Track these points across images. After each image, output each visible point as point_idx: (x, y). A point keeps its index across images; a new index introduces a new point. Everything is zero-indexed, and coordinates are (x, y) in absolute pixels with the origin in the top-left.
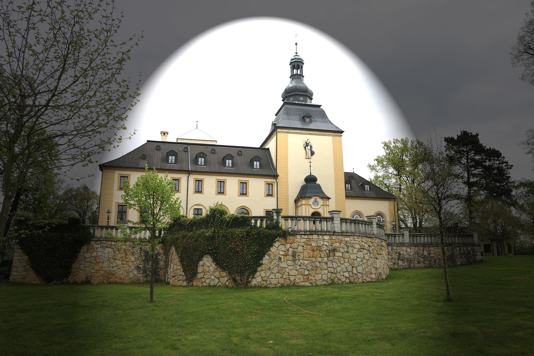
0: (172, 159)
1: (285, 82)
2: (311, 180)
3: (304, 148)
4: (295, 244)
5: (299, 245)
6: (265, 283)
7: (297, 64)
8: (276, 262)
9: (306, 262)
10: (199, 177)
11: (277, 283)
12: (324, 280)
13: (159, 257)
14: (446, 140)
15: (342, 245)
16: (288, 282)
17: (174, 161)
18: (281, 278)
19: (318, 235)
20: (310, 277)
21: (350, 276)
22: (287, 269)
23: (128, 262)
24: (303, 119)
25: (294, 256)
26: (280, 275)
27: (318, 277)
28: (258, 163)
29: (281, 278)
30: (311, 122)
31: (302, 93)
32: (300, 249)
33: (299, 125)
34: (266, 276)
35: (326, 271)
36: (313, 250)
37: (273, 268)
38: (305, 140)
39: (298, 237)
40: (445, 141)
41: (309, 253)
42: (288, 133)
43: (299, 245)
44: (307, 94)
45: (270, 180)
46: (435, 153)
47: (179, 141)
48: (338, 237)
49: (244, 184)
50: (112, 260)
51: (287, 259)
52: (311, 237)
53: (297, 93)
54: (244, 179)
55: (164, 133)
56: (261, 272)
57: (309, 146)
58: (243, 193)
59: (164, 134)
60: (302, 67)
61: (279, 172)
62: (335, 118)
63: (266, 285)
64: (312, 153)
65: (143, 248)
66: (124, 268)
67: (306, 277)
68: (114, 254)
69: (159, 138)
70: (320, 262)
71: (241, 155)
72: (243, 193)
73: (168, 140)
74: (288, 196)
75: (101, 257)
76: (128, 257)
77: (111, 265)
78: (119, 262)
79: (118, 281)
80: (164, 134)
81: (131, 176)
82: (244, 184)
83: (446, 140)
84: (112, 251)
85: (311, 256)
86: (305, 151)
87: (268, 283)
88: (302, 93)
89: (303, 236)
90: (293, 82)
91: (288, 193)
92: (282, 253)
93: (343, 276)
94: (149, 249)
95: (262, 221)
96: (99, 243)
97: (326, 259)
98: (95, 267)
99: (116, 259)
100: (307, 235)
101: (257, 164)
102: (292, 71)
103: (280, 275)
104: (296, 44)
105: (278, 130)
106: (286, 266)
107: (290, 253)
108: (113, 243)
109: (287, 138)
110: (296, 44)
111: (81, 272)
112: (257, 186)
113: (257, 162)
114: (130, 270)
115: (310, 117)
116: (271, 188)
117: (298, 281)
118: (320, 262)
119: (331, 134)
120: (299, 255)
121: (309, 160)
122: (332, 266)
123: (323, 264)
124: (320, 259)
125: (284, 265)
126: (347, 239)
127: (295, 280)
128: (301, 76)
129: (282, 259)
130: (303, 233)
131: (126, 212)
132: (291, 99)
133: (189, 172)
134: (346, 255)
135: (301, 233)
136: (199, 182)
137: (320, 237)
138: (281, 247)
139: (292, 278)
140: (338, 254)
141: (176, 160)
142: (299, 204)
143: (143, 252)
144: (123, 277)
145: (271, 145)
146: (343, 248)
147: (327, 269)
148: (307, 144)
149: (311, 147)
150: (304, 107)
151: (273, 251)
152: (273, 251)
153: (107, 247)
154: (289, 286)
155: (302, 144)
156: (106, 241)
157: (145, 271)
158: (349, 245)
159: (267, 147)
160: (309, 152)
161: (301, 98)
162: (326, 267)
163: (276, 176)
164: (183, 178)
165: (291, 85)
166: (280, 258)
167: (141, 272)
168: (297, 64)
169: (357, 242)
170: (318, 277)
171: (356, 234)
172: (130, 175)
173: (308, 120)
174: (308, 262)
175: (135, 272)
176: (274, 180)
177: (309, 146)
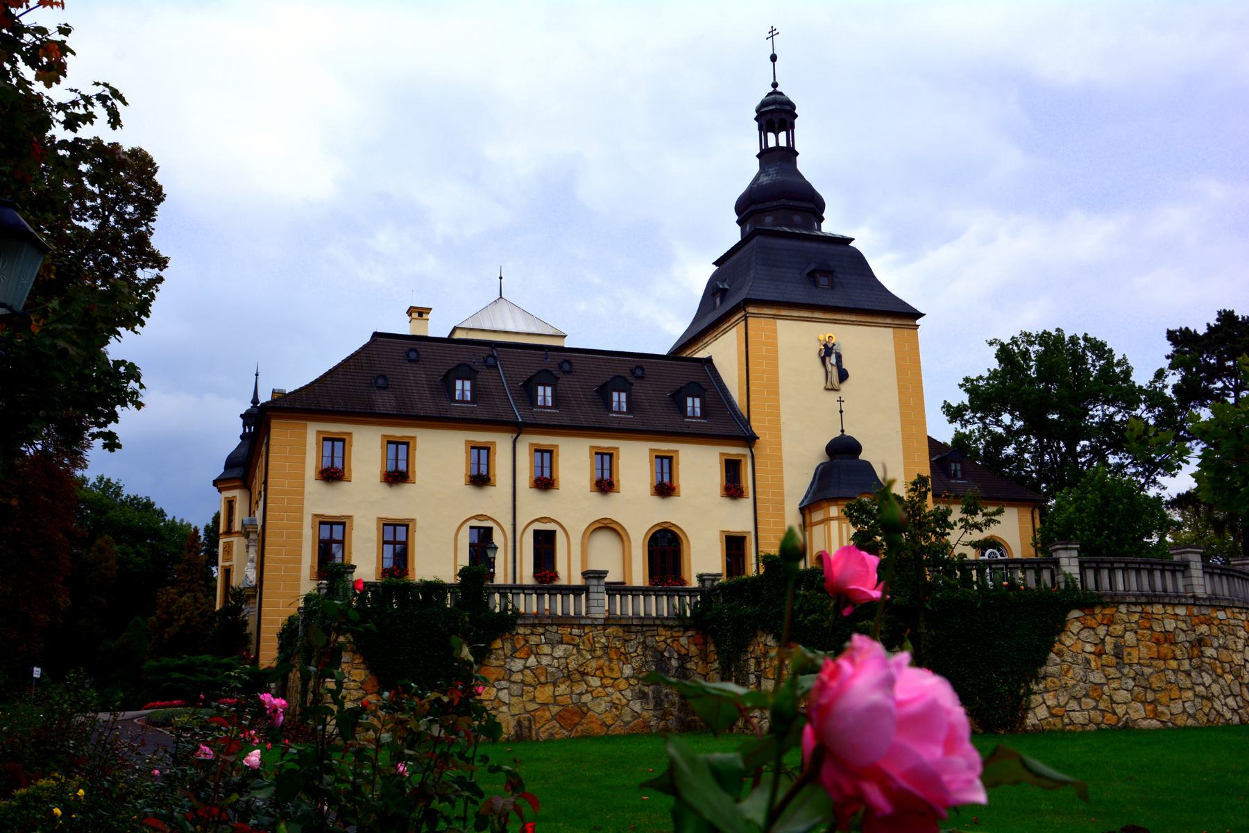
0: (463, 388)
1: (744, 170)
2: (843, 451)
3: (818, 362)
4: (1118, 627)
5: (1126, 630)
6: (1058, 721)
7: (776, 114)
8: (1078, 670)
9: (1147, 671)
10: (545, 441)
11: (1086, 721)
12: (1189, 715)
13: (689, 666)
14: (1171, 335)
15: (1215, 630)
16: (1111, 719)
17: (549, 399)
18: (1095, 708)
19: (1164, 605)
20: (1160, 708)
21: (1240, 708)
22: (1106, 688)
23: (615, 679)
24: (812, 277)
25: (1119, 656)
26: (1092, 703)
27: (1177, 708)
28: (468, 384)
29: (1095, 708)
30: (832, 286)
31: (798, 204)
32: (1130, 637)
33: (799, 296)
34: (1059, 705)
35: (1190, 694)
36: (1158, 642)
37: (1074, 686)
38: (823, 337)
39: (1123, 609)
40: (1169, 339)
41: (1149, 648)
42: (776, 317)
43: (1126, 630)
44: (811, 204)
45: (733, 451)
46: (1142, 378)
47: (459, 335)
48: (1204, 611)
49: (666, 462)
50: (578, 676)
51: (1104, 662)
52: (1149, 609)
53: (783, 201)
54: (664, 447)
55: (419, 313)
56: (1046, 696)
57: (833, 356)
58: (665, 489)
59: (420, 314)
60: (793, 127)
61: (756, 426)
62: (891, 273)
63: (1060, 726)
64: (843, 376)
65: (649, 641)
66: (607, 695)
67: (1150, 708)
68: (581, 661)
69: (402, 326)
70: (1174, 671)
71: (415, 361)
72: (665, 489)
73: (432, 333)
74: (782, 494)
75: (549, 669)
76: (616, 667)
77: (577, 689)
78: (595, 682)
79: (597, 729)
80: (420, 314)
81: (354, 437)
82: (666, 462)
83: (1171, 335)
84: (575, 651)
85: (1155, 655)
86: (822, 371)
87: (1066, 721)
88: (798, 204)
89: (1133, 608)
90: (771, 170)
91: (782, 487)
92: (1089, 648)
93: (1226, 705)
94: (663, 645)
95: (981, 572)
96: (541, 630)
97: (1186, 665)
98: (537, 694)
99: (588, 674)
100: (1140, 604)
101: (693, 405)
102: (763, 140)
103: (1092, 703)
104: (774, 58)
105: (751, 310)
106: (1104, 681)
107: (1109, 647)
108: (575, 631)
109: (775, 331)
110: (774, 58)
111: (504, 709)
112: (700, 465)
113: (669, 397)
114: (624, 701)
115: (828, 272)
116: (483, 460)
117: (1134, 716)
118: (1174, 671)
119: (889, 321)
120: (1129, 654)
121: (835, 396)
122: (1199, 681)
123: (1182, 676)
124: (1174, 664)
125: (1097, 677)
126: (1221, 615)
127: (1127, 713)
128: (789, 153)
129: (1093, 664)
130: (1133, 600)
131: (385, 542)
132: (769, 219)
133: (517, 428)
134: (1225, 655)
135: (1128, 600)
136: (546, 454)
137: (1169, 610)
138: (1085, 634)
139: (1120, 710)
140: (1209, 652)
141: (473, 390)
142: (817, 516)
143: (649, 653)
144: (609, 721)
145: (723, 351)
146: (1217, 637)
147: (1192, 689)
148: (828, 351)
149: (839, 357)
150: (807, 244)
151: (1068, 643)
152: (1068, 643)
153: (562, 643)
154: (1113, 729)
155: (817, 347)
156: (559, 625)
157: (658, 704)
158: (1225, 628)
159: (702, 354)
160: (834, 373)
161: (797, 219)
162: (1189, 684)
163: (749, 440)
164: (502, 443)
165: (764, 180)
166: (1088, 661)
167: (651, 706)
168: (776, 114)
169: (1240, 623)
170: (1177, 708)
171: (1237, 604)
172: (350, 434)
173: (823, 281)
174: (1151, 670)
175: (637, 706)
176: (746, 451)
177: (833, 356)
